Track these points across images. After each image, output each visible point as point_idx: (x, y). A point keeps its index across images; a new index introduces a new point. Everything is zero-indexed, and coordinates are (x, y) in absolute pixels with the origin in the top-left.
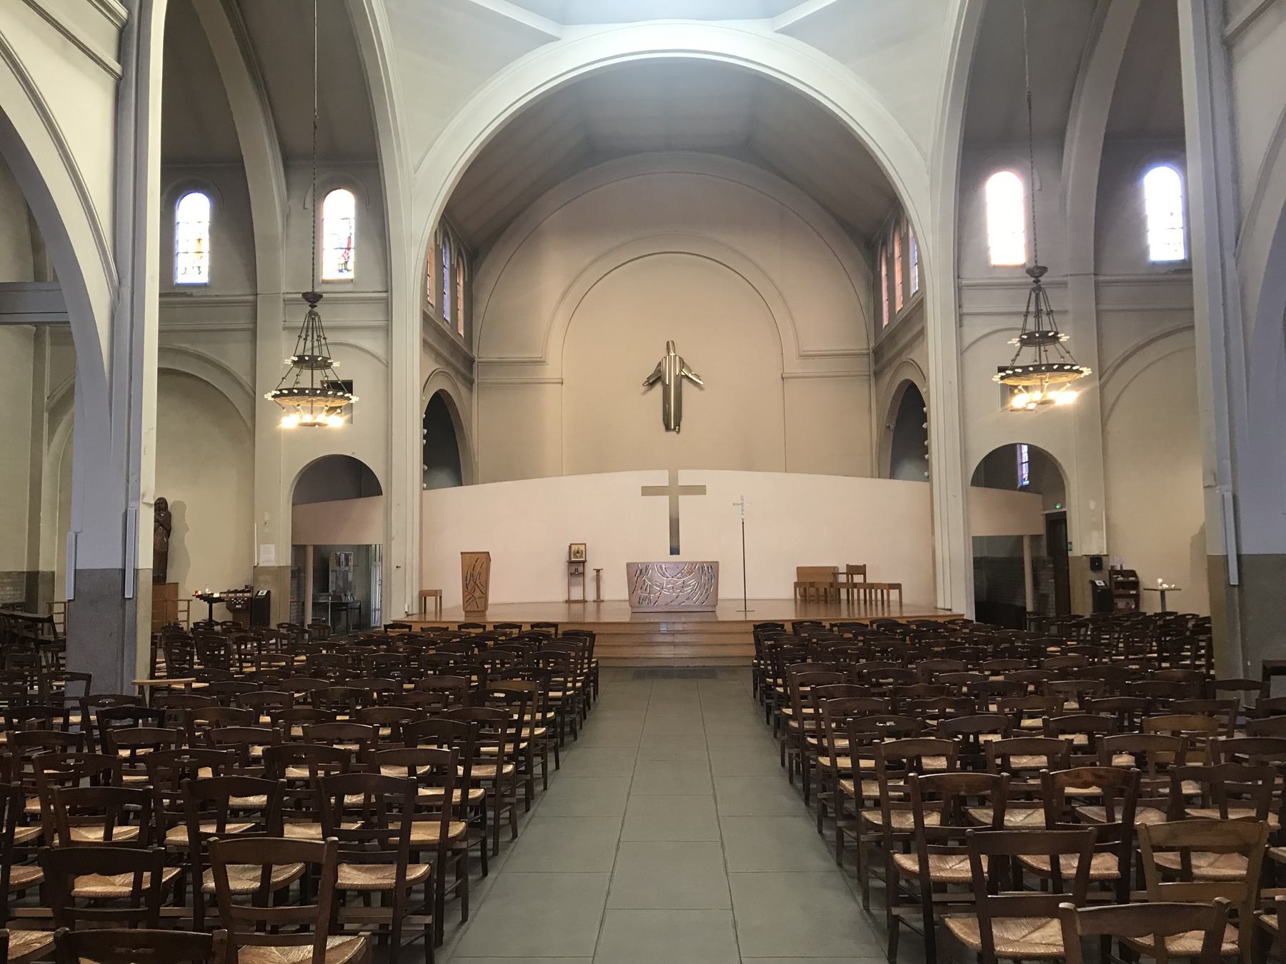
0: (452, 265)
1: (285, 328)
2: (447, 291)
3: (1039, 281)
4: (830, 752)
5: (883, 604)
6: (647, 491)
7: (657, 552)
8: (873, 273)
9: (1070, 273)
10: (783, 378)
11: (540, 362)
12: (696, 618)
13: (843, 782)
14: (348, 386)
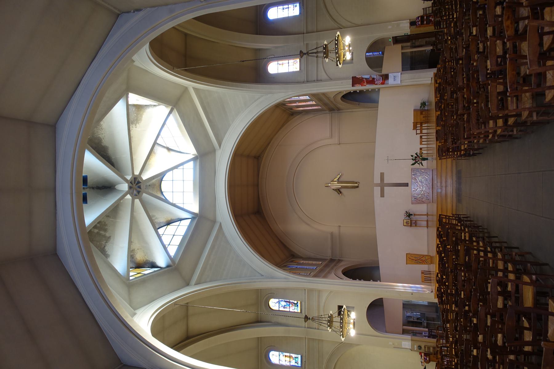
3: (309, 318)
4: (495, 129)
5: (429, 126)
6: (382, 195)
9: (303, 43)
10: (339, 144)
11: (332, 234)
12: (435, 177)
13: (509, 123)
14: (340, 307)
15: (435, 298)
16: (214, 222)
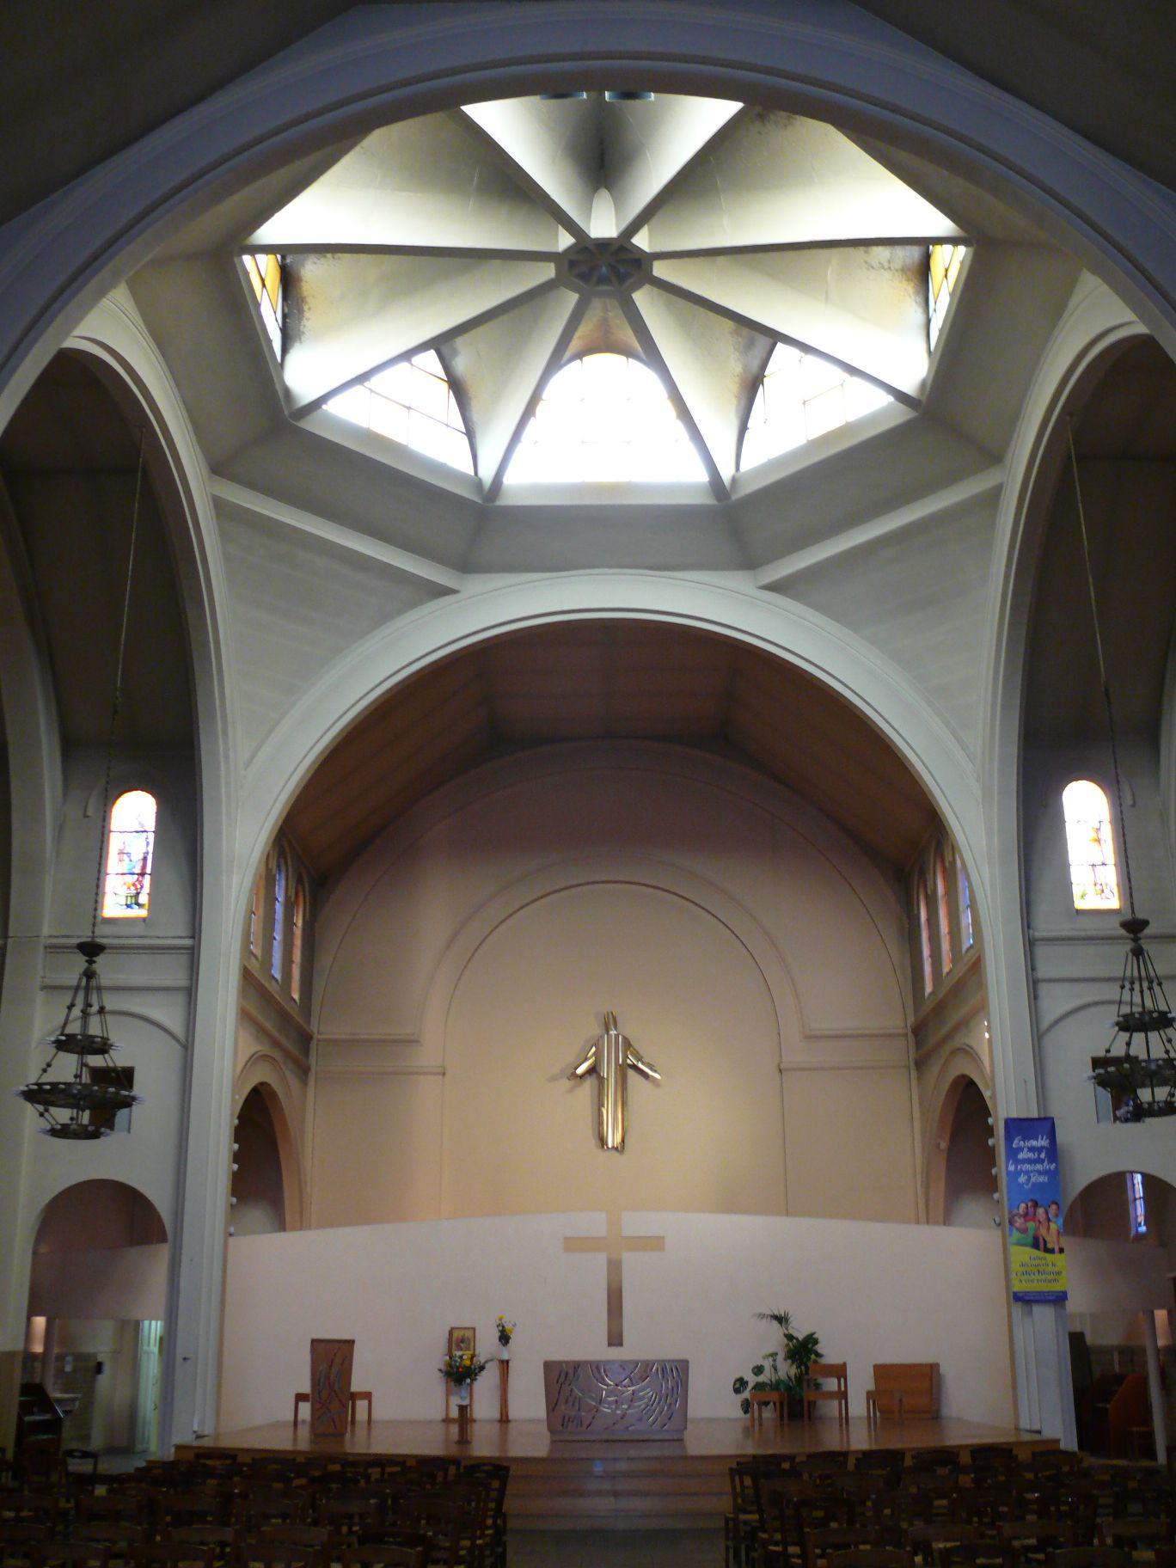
0: (287, 898)
1: (45, 988)
3: (95, 962)
7: (589, 1345)
8: (909, 917)
10: (780, 1070)
11: (412, 1041)
12: (653, 1451)
16: (467, 565)
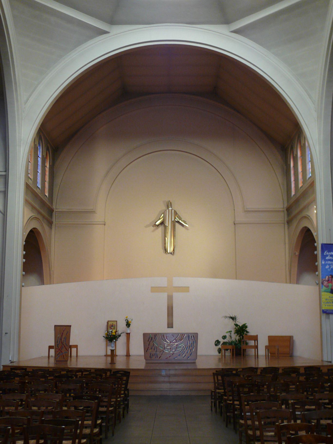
0: (43, 156)
2: (39, 171)
10: (235, 224)
11: (93, 212)
15: (3, 366)
16: (112, 21)
